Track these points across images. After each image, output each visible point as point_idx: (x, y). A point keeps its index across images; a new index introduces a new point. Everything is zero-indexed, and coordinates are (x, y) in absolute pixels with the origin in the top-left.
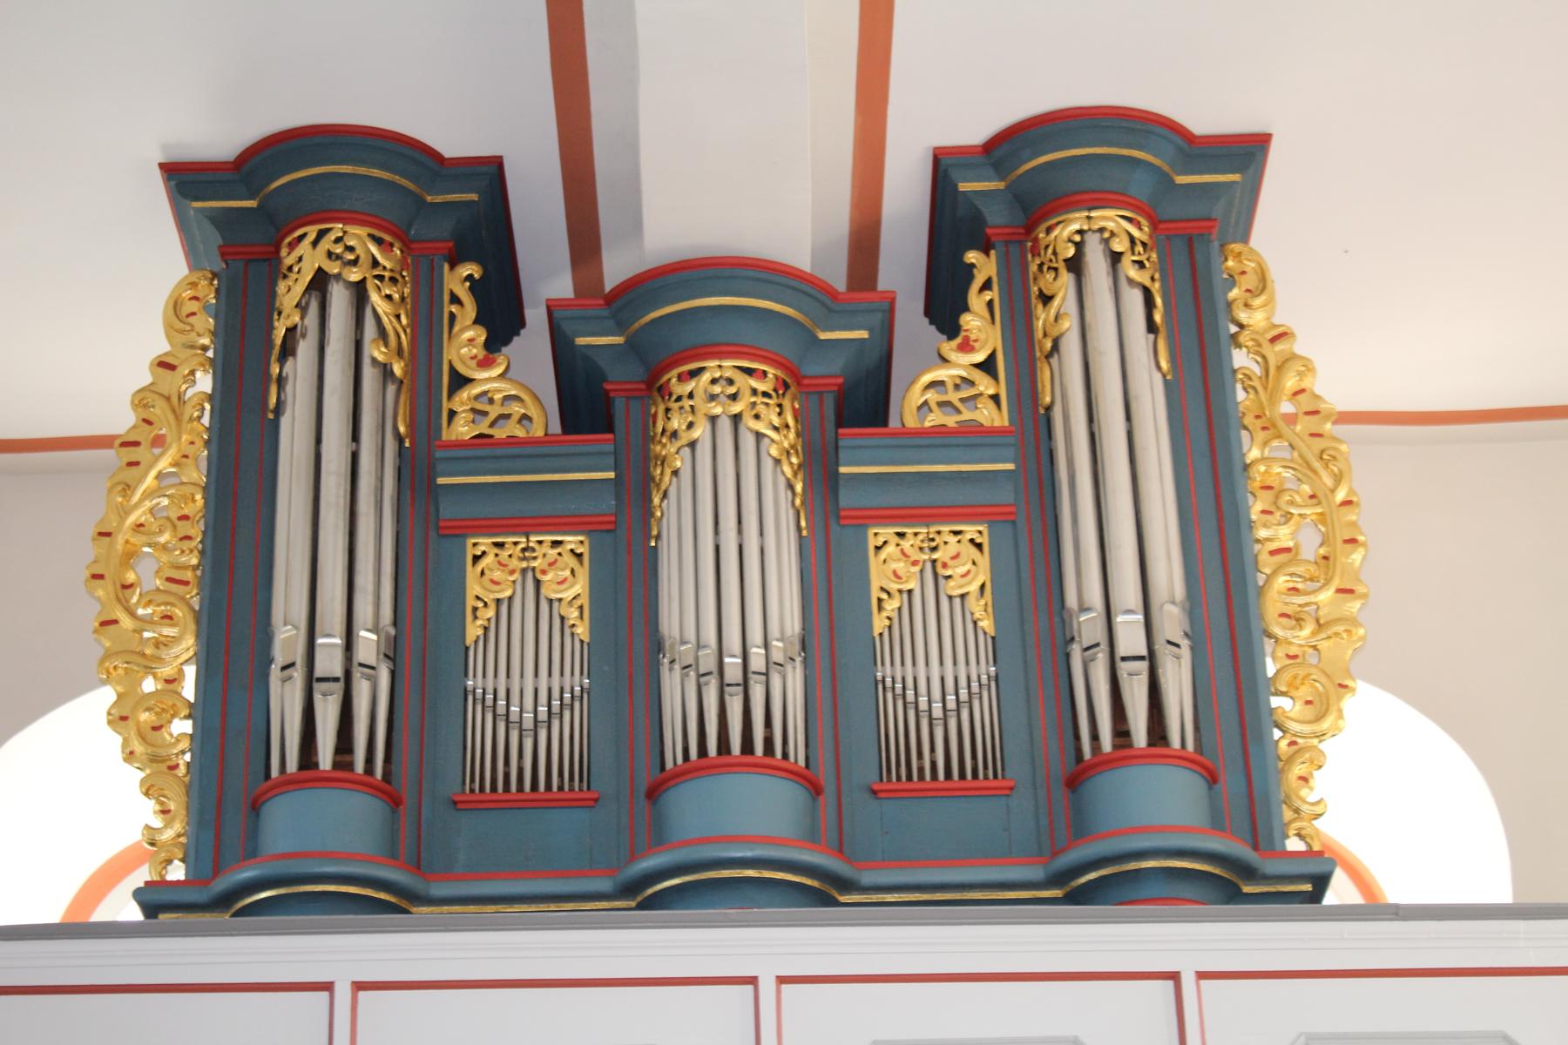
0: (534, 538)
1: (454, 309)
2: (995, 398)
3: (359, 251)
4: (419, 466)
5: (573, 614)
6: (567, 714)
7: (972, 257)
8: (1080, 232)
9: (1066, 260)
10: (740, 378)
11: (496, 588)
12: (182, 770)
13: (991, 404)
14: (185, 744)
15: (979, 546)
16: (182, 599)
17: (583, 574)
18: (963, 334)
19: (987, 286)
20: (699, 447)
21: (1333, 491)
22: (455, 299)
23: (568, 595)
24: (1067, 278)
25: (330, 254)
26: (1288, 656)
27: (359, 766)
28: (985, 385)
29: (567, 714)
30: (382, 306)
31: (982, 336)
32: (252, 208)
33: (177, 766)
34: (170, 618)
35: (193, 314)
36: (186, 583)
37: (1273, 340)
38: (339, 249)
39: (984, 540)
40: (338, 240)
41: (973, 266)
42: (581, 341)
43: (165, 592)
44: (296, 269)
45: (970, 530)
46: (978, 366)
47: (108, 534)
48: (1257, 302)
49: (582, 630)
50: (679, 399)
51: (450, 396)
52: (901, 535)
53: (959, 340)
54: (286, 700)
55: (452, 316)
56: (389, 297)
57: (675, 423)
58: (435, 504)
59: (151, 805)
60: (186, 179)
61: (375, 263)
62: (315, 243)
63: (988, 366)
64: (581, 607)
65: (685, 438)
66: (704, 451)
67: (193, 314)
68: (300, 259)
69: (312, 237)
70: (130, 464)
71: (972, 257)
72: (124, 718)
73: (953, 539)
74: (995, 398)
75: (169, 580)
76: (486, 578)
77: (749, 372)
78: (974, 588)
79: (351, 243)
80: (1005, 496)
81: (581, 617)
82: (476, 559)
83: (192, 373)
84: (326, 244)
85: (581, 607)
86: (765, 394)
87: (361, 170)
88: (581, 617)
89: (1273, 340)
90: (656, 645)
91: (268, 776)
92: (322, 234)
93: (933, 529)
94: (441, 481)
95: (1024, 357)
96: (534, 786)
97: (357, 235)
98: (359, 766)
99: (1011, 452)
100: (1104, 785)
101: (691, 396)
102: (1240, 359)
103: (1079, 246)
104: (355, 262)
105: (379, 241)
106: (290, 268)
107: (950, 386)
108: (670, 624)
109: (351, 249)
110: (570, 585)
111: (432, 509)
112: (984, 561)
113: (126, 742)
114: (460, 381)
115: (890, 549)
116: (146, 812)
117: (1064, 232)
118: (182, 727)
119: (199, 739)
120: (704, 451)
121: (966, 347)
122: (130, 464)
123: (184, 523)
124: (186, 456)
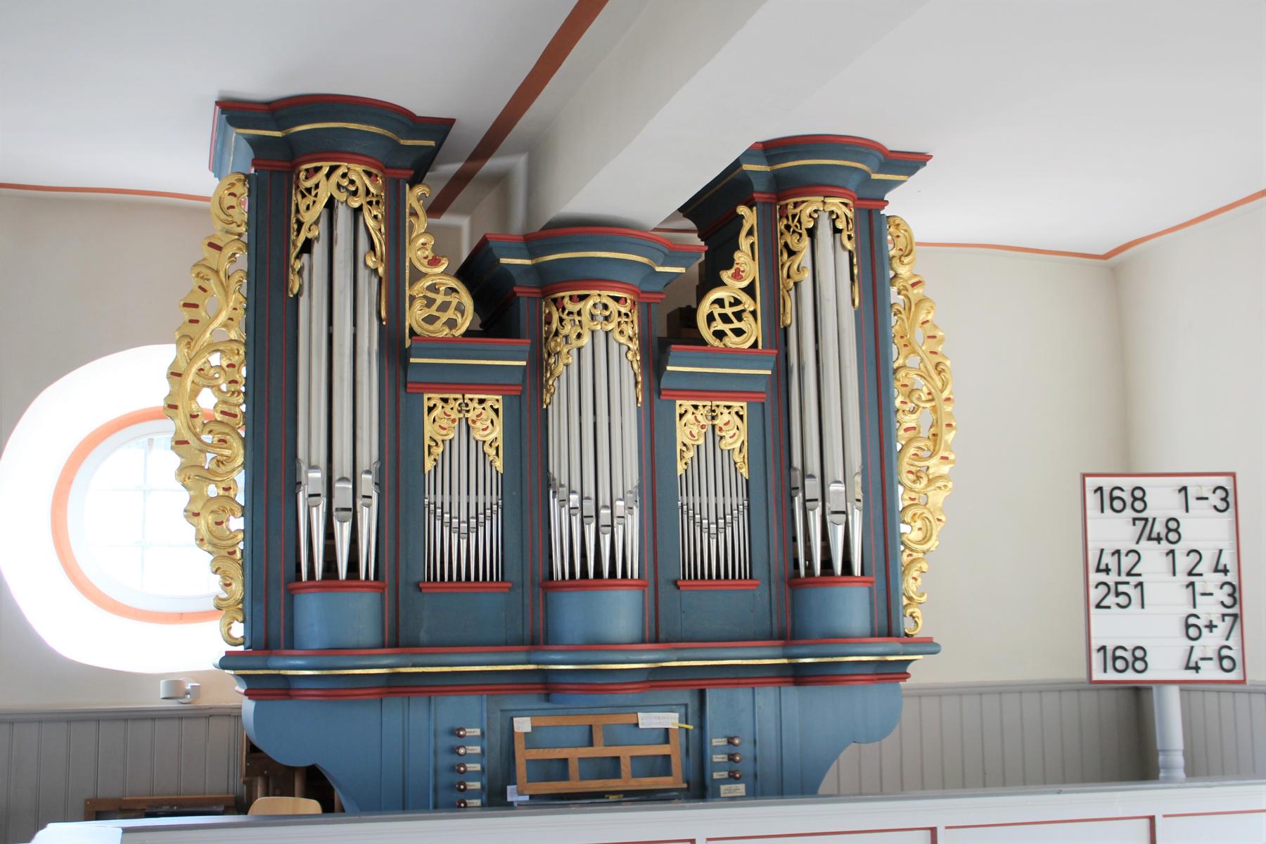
0: (468, 396)
1: (413, 220)
2: (754, 313)
3: (358, 183)
4: (395, 346)
5: (492, 452)
6: (488, 523)
7: (742, 210)
8: (816, 211)
9: (807, 230)
10: (611, 303)
11: (444, 432)
12: (238, 555)
13: (751, 318)
14: (241, 536)
15: (741, 417)
16: (234, 430)
17: (499, 423)
18: (735, 266)
19: (750, 233)
20: (583, 351)
21: (942, 391)
22: (414, 214)
23: (489, 439)
24: (806, 241)
25: (339, 186)
26: (911, 499)
27: (363, 576)
28: (748, 304)
29: (488, 523)
30: (371, 223)
31: (747, 269)
32: (281, 140)
33: (234, 552)
34: (224, 441)
35: (232, 207)
36: (235, 416)
37: (913, 285)
38: (345, 182)
39: (744, 413)
40: (344, 176)
41: (742, 217)
42: (503, 261)
43: (221, 422)
44: (313, 193)
45: (736, 405)
46: (743, 290)
47: (179, 375)
48: (906, 260)
49: (499, 464)
50: (570, 313)
51: (411, 284)
52: (696, 407)
53: (732, 271)
54: (312, 517)
55: (412, 226)
56: (376, 217)
57: (568, 329)
58: (403, 365)
59: (217, 578)
60: (234, 112)
61: (368, 192)
62: (328, 176)
63: (750, 290)
64: (497, 448)
65: (575, 343)
66: (587, 354)
67: (232, 207)
68: (317, 186)
69: (325, 170)
70: (192, 321)
71: (742, 210)
72: (197, 515)
73: (726, 411)
74: (754, 313)
75: (223, 413)
76: (437, 424)
77: (617, 299)
78: (738, 445)
79: (354, 178)
80: (761, 387)
81: (497, 454)
82: (430, 409)
83: (234, 254)
84: (336, 177)
85: (497, 448)
86: (627, 315)
87: (364, 127)
88: (497, 454)
89: (913, 285)
90: (546, 482)
91: (299, 578)
92: (333, 169)
93: (715, 403)
94: (412, 360)
95: (771, 289)
96: (468, 578)
97: (357, 172)
98: (363, 576)
99: (771, 365)
100: (814, 595)
101: (579, 313)
102: (895, 297)
103: (816, 220)
104: (355, 193)
105: (369, 174)
106: (309, 190)
107: (727, 304)
108: (558, 466)
109: (352, 182)
110: (490, 429)
111: (402, 374)
112: (744, 427)
113: (198, 531)
114: (417, 275)
115: (689, 417)
116: (214, 585)
117: (810, 206)
118: (237, 523)
119: (252, 532)
120: (587, 354)
121: (737, 276)
122: (192, 321)
123: (231, 369)
124: (231, 319)
